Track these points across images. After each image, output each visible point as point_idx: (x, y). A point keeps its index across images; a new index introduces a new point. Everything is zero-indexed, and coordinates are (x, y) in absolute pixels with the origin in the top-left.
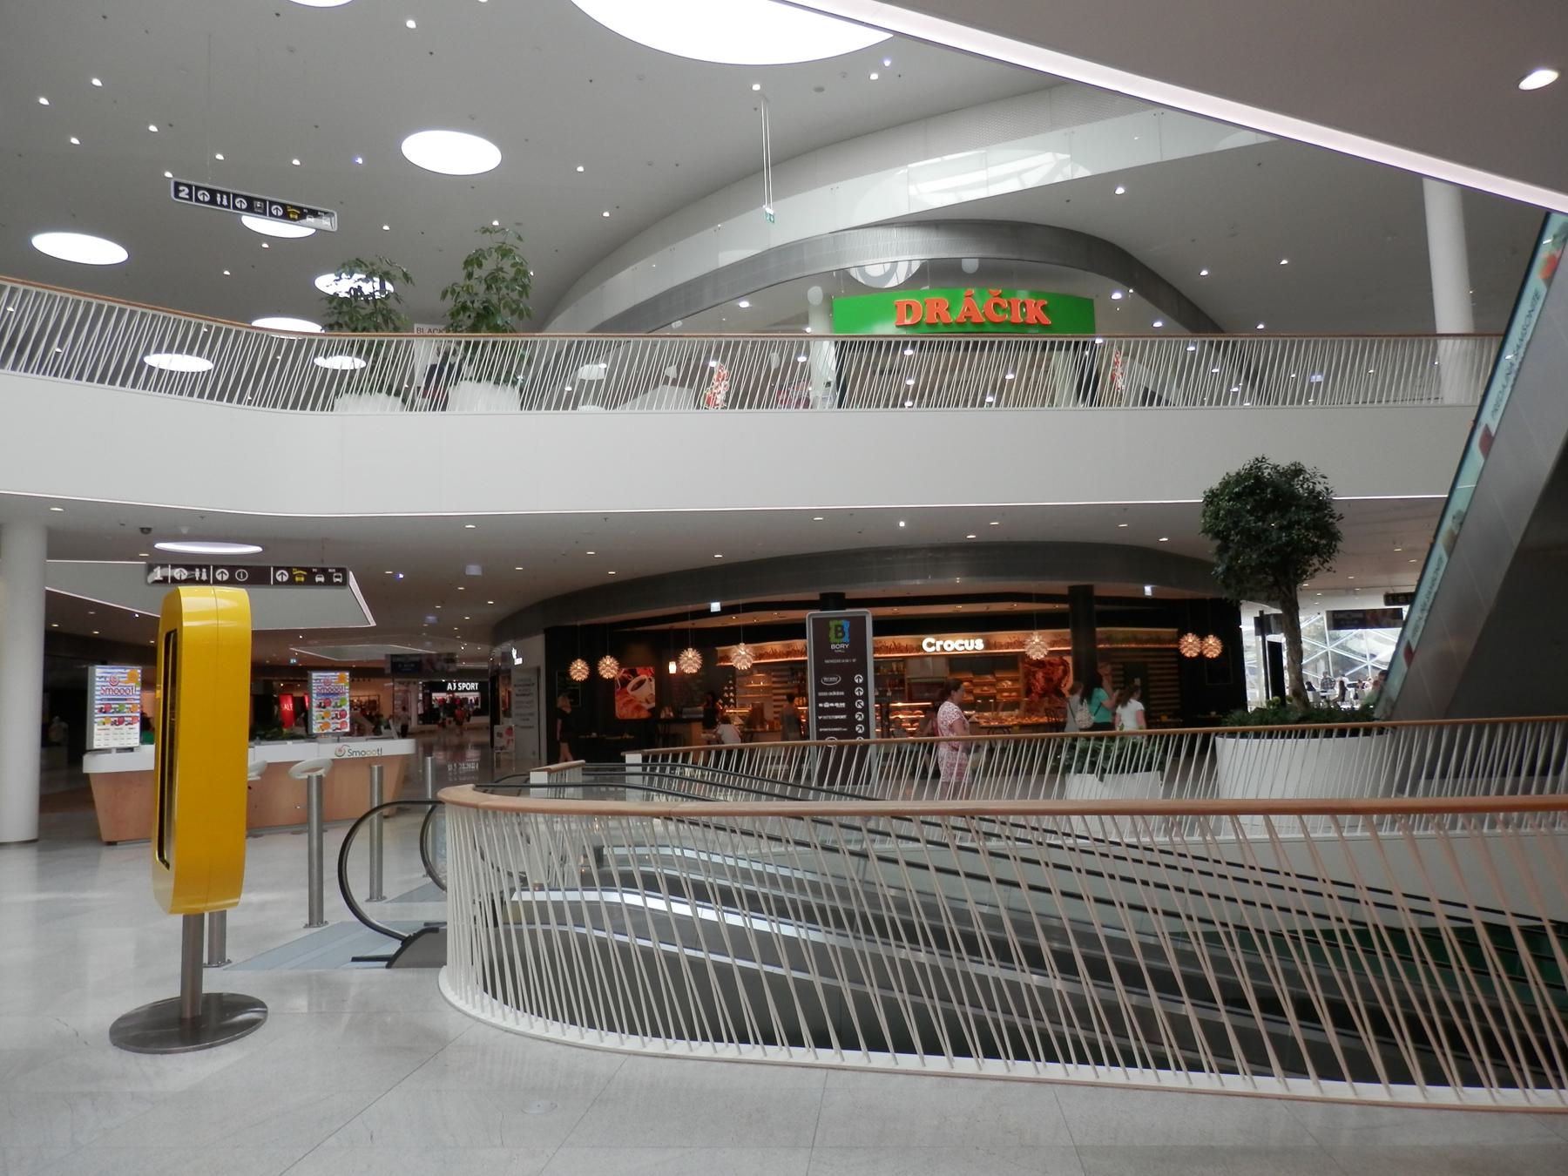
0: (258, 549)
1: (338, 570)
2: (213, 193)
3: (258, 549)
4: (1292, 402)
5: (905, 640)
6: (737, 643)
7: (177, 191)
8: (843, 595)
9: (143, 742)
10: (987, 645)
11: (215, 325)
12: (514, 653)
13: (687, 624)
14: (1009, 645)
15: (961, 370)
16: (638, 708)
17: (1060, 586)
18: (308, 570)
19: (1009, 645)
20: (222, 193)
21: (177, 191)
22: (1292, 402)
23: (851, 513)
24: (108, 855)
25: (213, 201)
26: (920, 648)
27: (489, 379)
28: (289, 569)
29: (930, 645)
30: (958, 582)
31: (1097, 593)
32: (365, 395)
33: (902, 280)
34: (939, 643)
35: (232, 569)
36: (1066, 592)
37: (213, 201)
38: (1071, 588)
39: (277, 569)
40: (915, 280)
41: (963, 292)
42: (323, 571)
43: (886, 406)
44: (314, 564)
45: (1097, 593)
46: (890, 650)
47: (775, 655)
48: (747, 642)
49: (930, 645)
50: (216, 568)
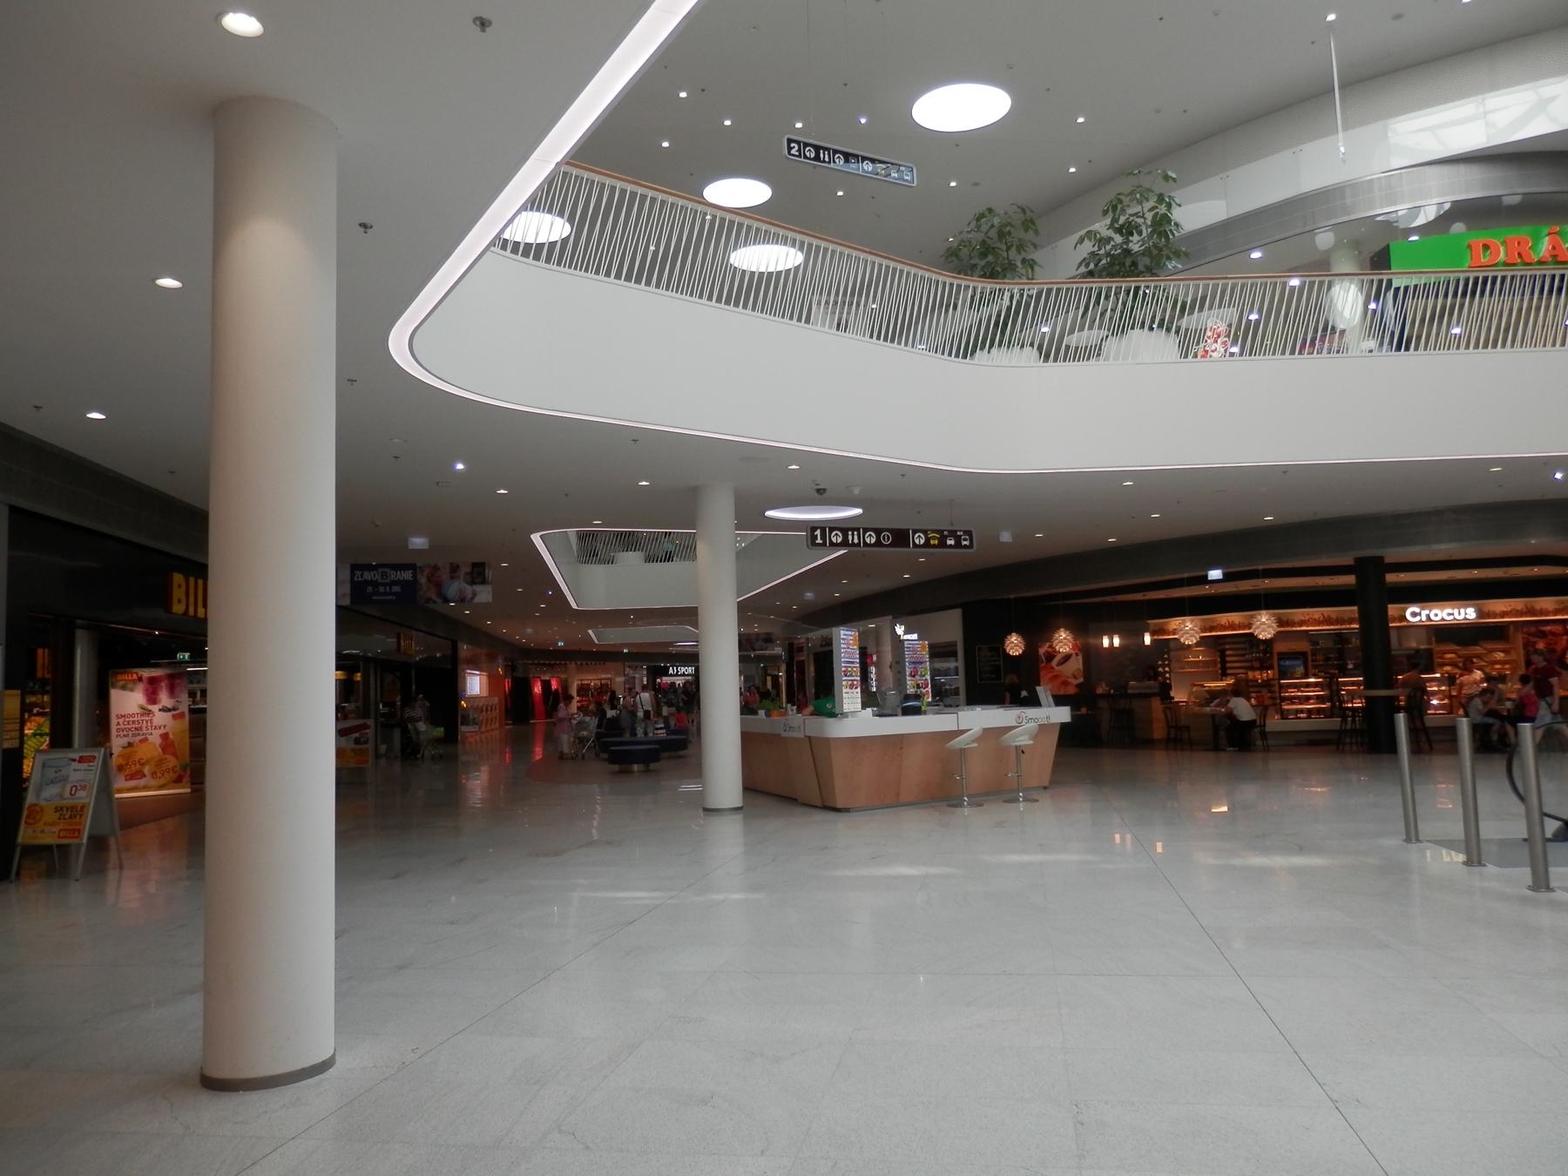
0: (858, 511)
1: (966, 532)
2: (817, 148)
3: (858, 511)
4: (1485, 346)
5: (1235, 617)
6: (1260, 609)
7: (790, 149)
8: (1382, 558)
9: (864, 706)
10: (1480, 614)
11: (1385, 278)
12: (900, 630)
13: (1109, 599)
14: (1504, 614)
15: (1520, 310)
16: (1065, 683)
17: (1347, 559)
18: (940, 532)
19: (1504, 614)
20: (825, 149)
21: (790, 149)
22: (1485, 346)
23: (1285, 470)
24: (840, 823)
25: (817, 158)
26: (1404, 618)
27: (1142, 327)
28: (925, 532)
29: (1414, 614)
30: (1535, 543)
31: (1387, 560)
32: (1017, 349)
33: (1431, 217)
34: (1424, 613)
35: (845, 531)
36: (1351, 562)
37: (817, 158)
38: (1357, 560)
39: (915, 532)
40: (1443, 221)
41: (1546, 230)
42: (953, 534)
43: (1292, 353)
44: (946, 526)
45: (1387, 560)
46: (1224, 628)
47: (1232, 626)
48: (1267, 608)
49: (1414, 614)
50: (832, 530)
